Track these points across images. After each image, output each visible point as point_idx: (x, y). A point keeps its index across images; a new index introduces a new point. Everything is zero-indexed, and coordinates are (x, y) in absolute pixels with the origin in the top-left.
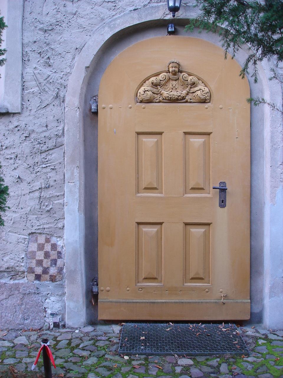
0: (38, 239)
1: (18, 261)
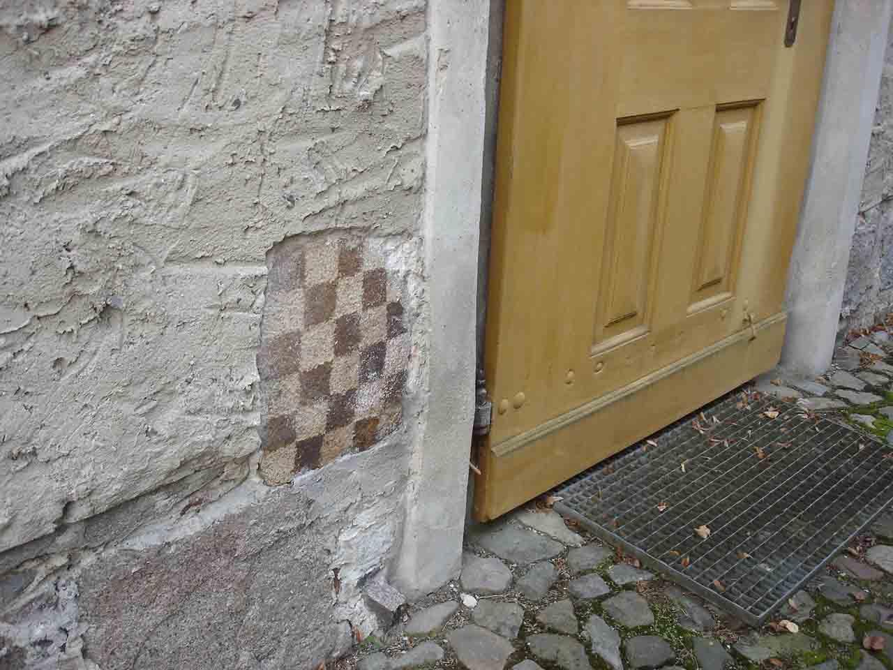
0: (309, 265)
1: (232, 411)
